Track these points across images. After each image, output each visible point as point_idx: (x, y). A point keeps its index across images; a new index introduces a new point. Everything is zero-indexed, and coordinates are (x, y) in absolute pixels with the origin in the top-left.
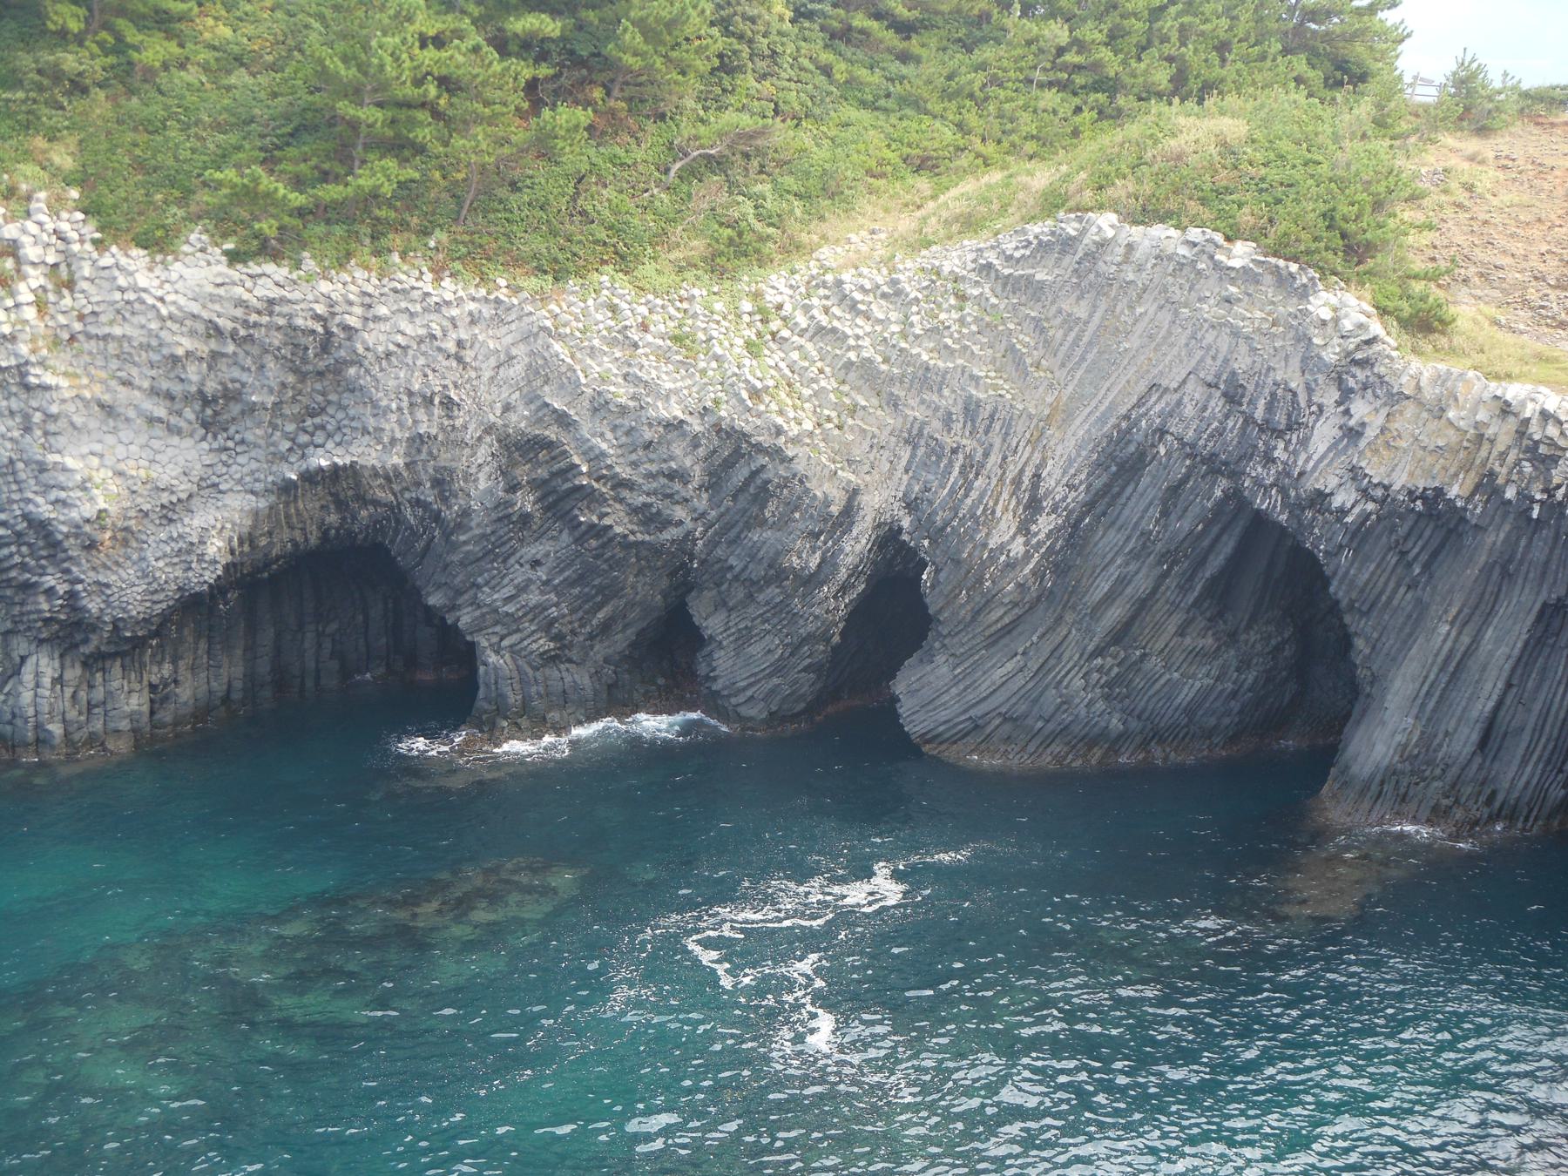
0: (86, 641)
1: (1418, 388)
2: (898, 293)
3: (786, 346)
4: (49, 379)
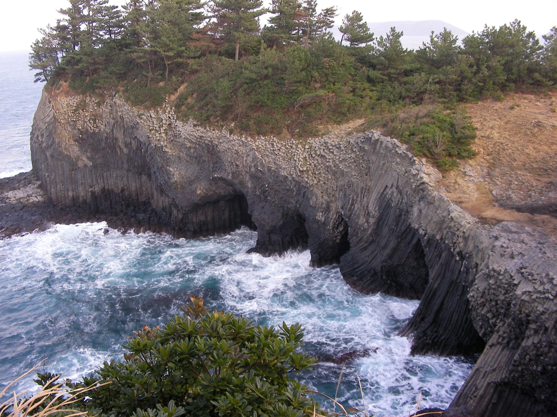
2: (340, 147)
4: (167, 150)
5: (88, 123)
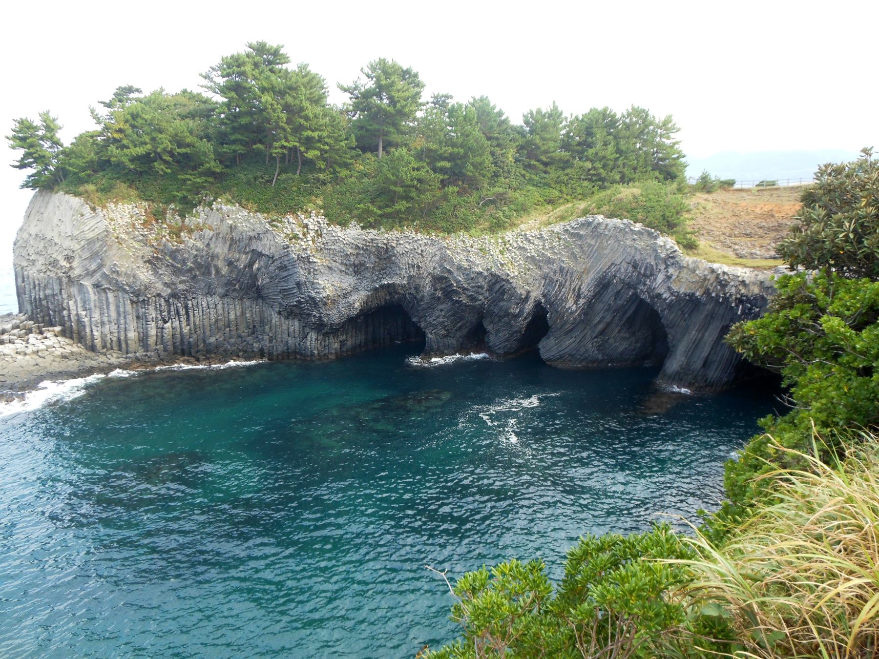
4: (315, 260)
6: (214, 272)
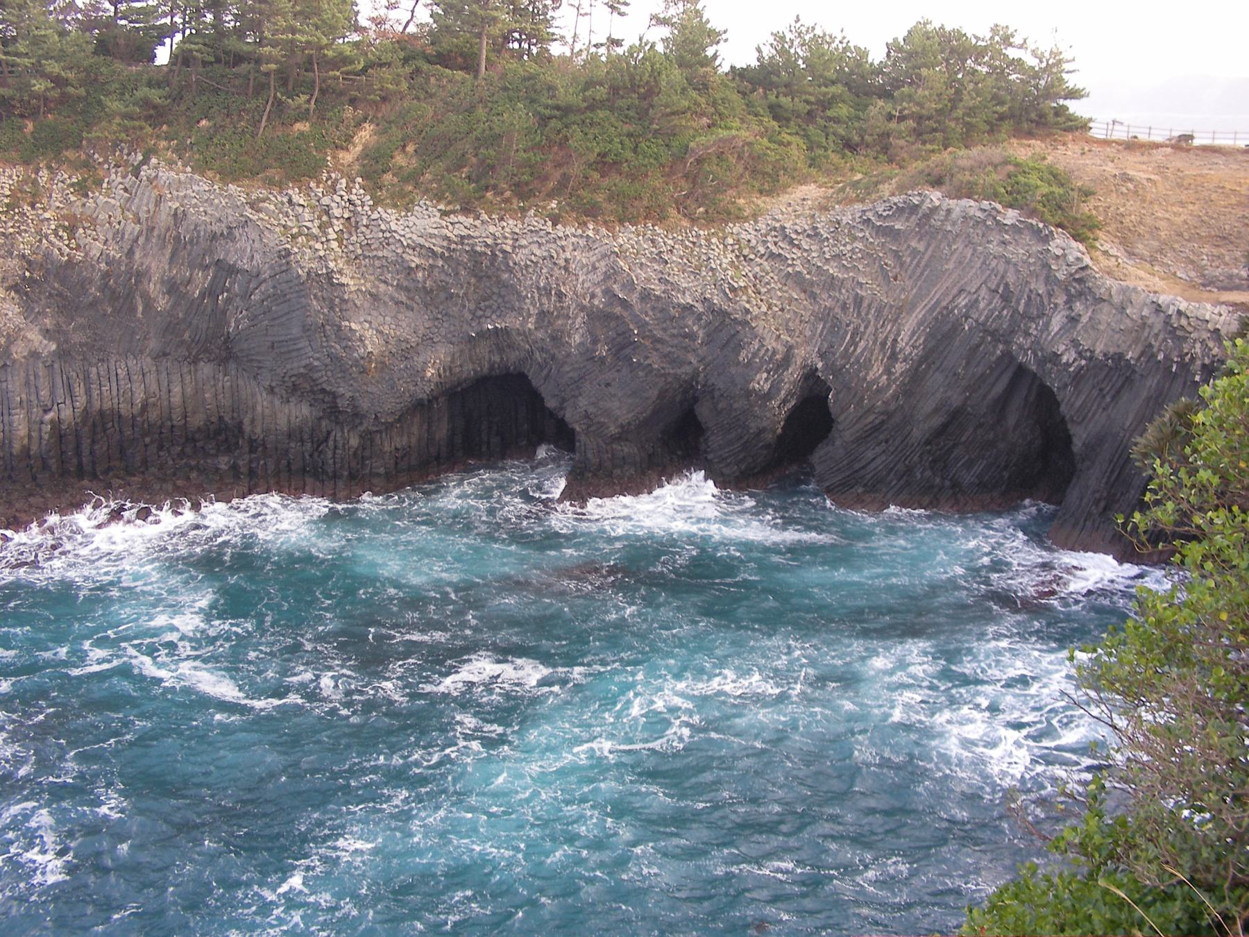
0: (361, 424)
1: (1110, 295)
2: (817, 234)
3: (752, 263)
4: (344, 280)
5: (52, 238)
6: (140, 308)
